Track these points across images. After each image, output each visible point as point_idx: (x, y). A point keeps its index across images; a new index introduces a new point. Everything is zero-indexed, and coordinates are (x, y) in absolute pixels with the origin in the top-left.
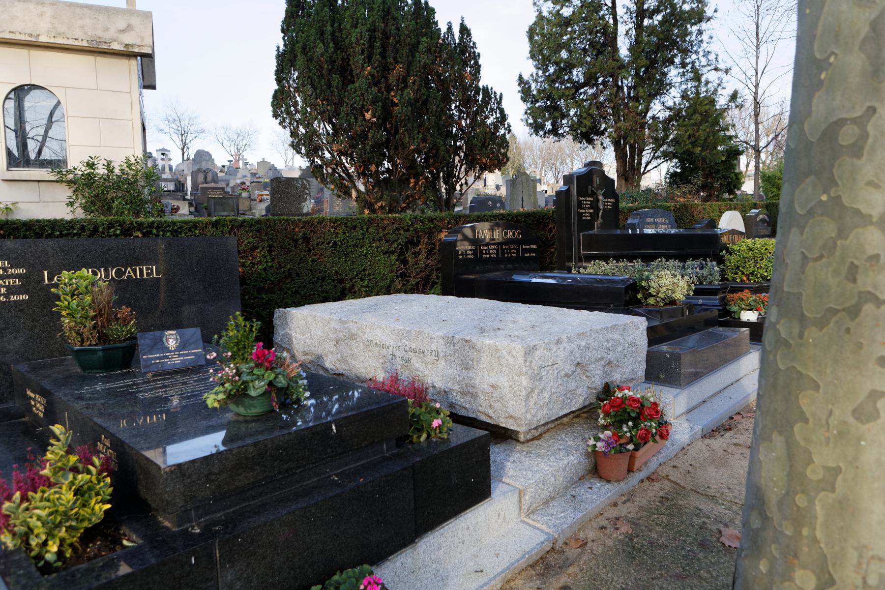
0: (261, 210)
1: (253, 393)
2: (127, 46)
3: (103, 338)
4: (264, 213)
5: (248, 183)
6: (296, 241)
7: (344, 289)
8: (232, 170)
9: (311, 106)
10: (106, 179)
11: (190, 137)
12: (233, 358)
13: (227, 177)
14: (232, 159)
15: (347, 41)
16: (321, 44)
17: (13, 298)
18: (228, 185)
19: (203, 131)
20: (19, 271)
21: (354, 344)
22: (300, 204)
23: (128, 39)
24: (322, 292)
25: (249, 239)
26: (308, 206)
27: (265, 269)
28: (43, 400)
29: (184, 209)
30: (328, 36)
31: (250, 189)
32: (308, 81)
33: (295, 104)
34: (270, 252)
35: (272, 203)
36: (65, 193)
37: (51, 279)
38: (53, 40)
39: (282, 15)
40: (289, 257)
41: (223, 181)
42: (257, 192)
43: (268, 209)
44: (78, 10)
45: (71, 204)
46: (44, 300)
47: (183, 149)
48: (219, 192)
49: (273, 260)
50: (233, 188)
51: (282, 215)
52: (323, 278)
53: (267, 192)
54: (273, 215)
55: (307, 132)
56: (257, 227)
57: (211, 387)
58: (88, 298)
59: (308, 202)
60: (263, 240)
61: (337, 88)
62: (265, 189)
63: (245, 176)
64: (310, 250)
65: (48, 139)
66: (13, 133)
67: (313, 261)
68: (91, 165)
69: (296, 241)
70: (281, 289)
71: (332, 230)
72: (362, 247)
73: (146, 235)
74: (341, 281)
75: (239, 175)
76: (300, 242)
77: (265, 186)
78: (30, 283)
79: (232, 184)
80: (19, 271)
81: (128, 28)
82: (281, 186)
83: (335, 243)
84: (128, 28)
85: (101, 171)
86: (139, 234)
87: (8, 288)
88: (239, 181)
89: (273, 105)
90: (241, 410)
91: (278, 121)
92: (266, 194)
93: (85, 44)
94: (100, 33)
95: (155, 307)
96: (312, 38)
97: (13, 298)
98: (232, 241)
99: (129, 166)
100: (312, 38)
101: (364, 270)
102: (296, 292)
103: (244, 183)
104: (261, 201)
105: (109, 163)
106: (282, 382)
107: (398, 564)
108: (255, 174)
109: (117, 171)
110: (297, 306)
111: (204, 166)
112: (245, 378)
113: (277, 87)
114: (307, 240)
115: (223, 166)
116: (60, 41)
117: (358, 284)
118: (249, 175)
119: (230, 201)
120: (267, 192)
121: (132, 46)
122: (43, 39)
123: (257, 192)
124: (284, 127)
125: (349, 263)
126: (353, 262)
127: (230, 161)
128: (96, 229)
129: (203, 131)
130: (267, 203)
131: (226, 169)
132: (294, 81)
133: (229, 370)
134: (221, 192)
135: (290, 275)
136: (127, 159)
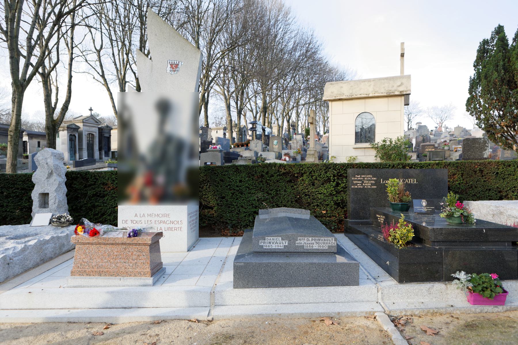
0: (456, 157)
1: (455, 216)
2: (401, 92)
3: (401, 201)
4: (458, 158)
5: (448, 141)
6: (476, 172)
7: (502, 196)
8: (438, 133)
9: (488, 104)
10: (390, 146)
11: (413, 115)
12: (449, 205)
13: (435, 138)
14: (437, 126)
15: (513, 67)
16: (496, 73)
17: (373, 187)
18: (436, 142)
19: (420, 111)
20: (375, 179)
21: (502, 216)
22: (481, 152)
23: (401, 89)
24: (489, 196)
25: (452, 170)
26: (488, 153)
27: (459, 184)
28: (384, 217)
29: (414, 157)
30: (500, 67)
31: (450, 144)
32: (486, 91)
33: (480, 103)
34: (462, 176)
35: (463, 151)
36: (374, 152)
37: (383, 182)
38: (374, 95)
39: (475, 58)
40: (472, 178)
41: (433, 140)
42: (454, 146)
43: (460, 156)
44: (383, 81)
45: (376, 156)
46: (382, 189)
47: (408, 123)
48: (431, 147)
49: (464, 180)
50: (439, 144)
51: (469, 159)
52: (490, 190)
53: (460, 146)
54: (464, 159)
55: (486, 117)
56: (456, 165)
57: (441, 212)
58: (397, 188)
59: (487, 151)
60: (459, 171)
61: (505, 93)
62: (459, 144)
63: (446, 137)
64: (483, 176)
65: (21, 22)
66: (33, 37)
67: (484, 181)
68: (384, 141)
69: (476, 172)
70: (466, 193)
71: (496, 167)
72: (513, 175)
73: (411, 168)
74: (500, 192)
75: (442, 136)
76: (478, 172)
77: (459, 142)
78: (377, 183)
79: (438, 142)
80: (375, 179)
81: (402, 84)
82: (470, 144)
83: (497, 173)
84: (402, 84)
85: (388, 143)
86: (408, 168)
87: (371, 184)
88: (442, 140)
89: (466, 105)
90: (451, 221)
91: (469, 113)
92: (460, 147)
93: (385, 94)
94: (390, 89)
95: (418, 192)
96: (491, 71)
97: (373, 187)
98: (445, 171)
99: (399, 140)
100: (491, 71)
101: (515, 187)
102: (475, 195)
103: (446, 141)
104: (456, 151)
105: (391, 139)
106: (465, 214)
107: (509, 284)
108: (453, 135)
109: (394, 143)
110: (474, 201)
111: (424, 133)
112: (453, 211)
113: (469, 96)
114: (481, 171)
115: (432, 131)
116: (376, 95)
117: (511, 194)
118: (449, 136)
119: (441, 153)
120: (460, 146)
121: (403, 91)
122: (371, 95)
123: (454, 146)
124: (473, 116)
125: (505, 183)
126: (508, 183)
127: (436, 127)
128: (394, 166)
129: (420, 111)
130: (460, 152)
131: (433, 132)
132: (479, 92)
133: (448, 208)
134: (433, 147)
135: (472, 187)
136: (398, 137)
